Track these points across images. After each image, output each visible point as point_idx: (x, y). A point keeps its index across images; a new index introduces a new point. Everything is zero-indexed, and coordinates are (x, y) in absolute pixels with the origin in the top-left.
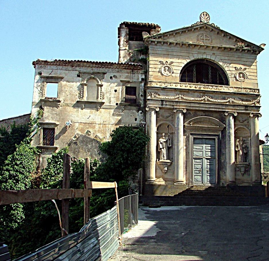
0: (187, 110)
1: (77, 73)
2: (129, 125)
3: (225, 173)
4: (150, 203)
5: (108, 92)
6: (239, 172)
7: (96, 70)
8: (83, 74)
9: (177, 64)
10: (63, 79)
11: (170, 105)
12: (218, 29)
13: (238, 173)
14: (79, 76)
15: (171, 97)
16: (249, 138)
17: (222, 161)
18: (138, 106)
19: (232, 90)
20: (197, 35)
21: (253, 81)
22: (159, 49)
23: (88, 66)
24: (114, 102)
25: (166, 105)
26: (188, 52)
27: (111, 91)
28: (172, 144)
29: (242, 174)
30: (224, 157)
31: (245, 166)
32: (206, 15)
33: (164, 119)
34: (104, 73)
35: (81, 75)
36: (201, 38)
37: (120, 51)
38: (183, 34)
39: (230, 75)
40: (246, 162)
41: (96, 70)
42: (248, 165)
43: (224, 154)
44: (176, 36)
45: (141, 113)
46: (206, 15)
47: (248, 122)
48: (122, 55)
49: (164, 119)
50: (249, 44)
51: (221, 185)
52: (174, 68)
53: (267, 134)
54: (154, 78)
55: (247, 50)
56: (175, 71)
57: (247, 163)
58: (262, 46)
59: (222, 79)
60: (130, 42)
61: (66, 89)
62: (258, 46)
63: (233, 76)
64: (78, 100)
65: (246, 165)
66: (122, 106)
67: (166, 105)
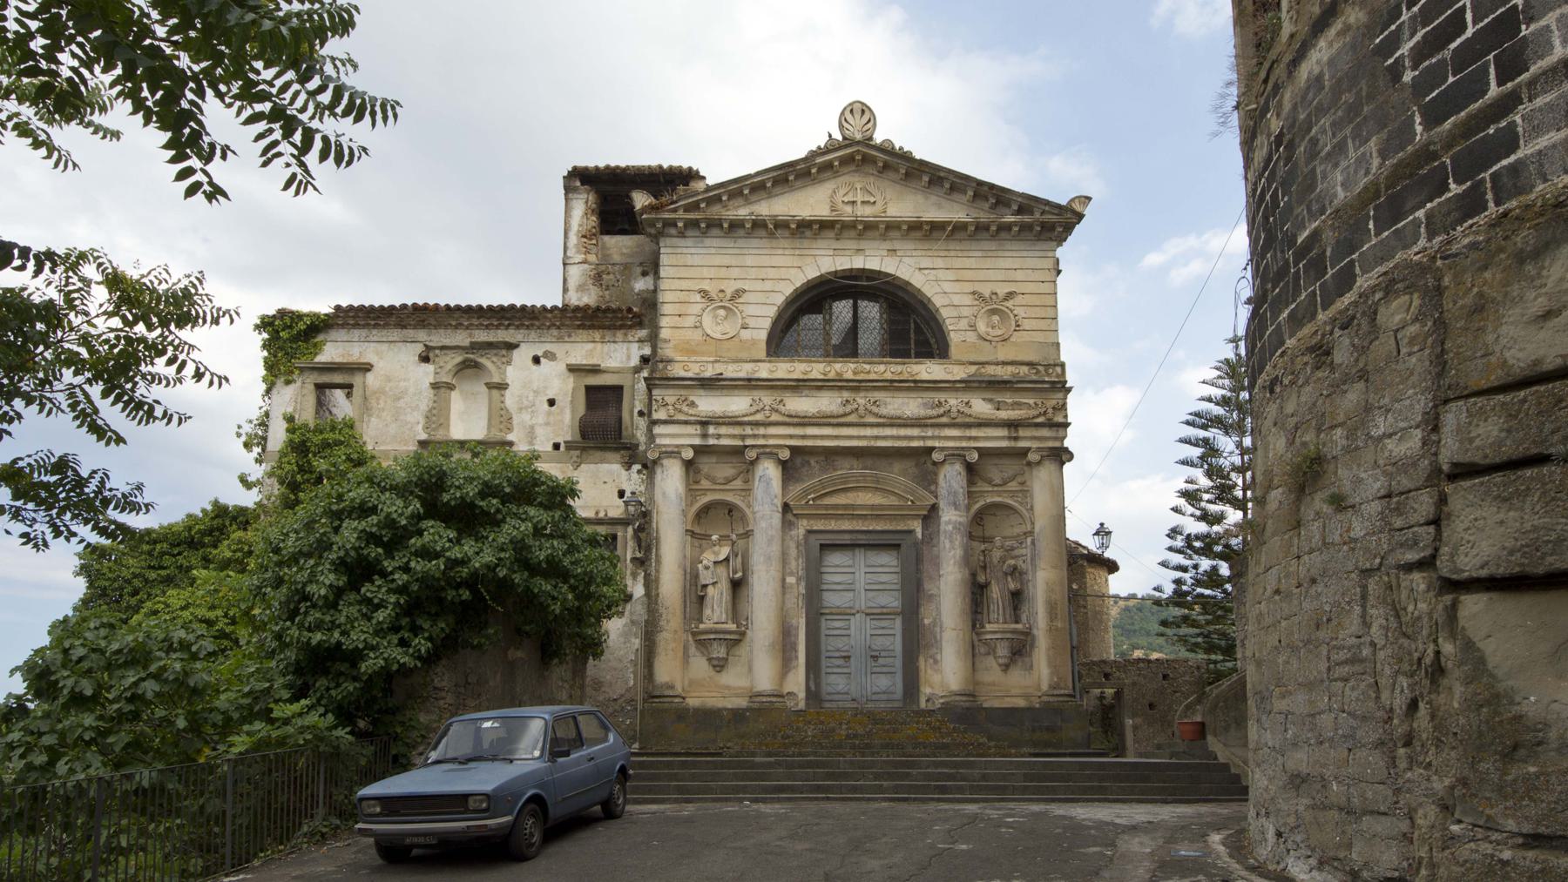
0: (793, 449)
1: (419, 348)
2: (597, 513)
3: (936, 662)
4: (90, 671)
5: (526, 408)
6: (991, 658)
7: (482, 336)
8: (437, 352)
9: (760, 298)
10: (369, 370)
11: (734, 436)
12: (906, 157)
13: (990, 662)
14: (425, 359)
15: (738, 404)
16: (1029, 540)
17: (926, 621)
18: (629, 449)
19: (959, 373)
20: (830, 191)
21: (1039, 337)
22: (693, 250)
23: (454, 323)
24: (548, 440)
25: (719, 436)
26: (797, 252)
27: (537, 402)
28: (745, 567)
29: (1000, 665)
30: (933, 606)
31: (1009, 636)
32: (863, 111)
33: (718, 487)
34: (511, 347)
35: (431, 355)
36: (846, 200)
37: (568, 267)
38: (778, 190)
39: (953, 321)
40: (1017, 622)
41: (482, 336)
42: (1022, 633)
43: (931, 595)
44: (754, 198)
45: (639, 472)
46: (863, 111)
47: (1023, 484)
48: (572, 284)
49: (718, 487)
50: (1028, 204)
51: (923, 705)
52: (750, 310)
53: (1102, 524)
54: (676, 348)
55: (1015, 224)
56: (752, 322)
57: (1019, 626)
58: (1077, 207)
59: (927, 343)
60: (606, 238)
61: (382, 406)
62: (1059, 206)
63: (963, 324)
64: (424, 436)
65: (1014, 632)
66: (572, 452)
67: (719, 436)
